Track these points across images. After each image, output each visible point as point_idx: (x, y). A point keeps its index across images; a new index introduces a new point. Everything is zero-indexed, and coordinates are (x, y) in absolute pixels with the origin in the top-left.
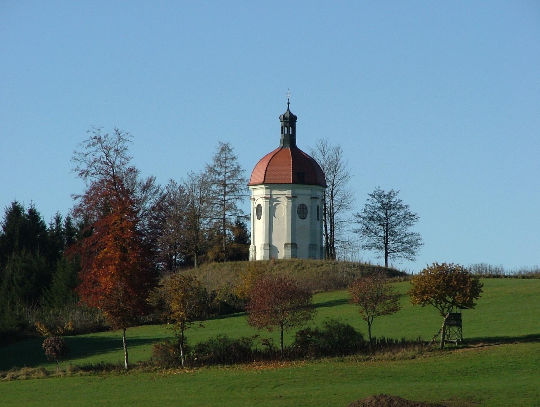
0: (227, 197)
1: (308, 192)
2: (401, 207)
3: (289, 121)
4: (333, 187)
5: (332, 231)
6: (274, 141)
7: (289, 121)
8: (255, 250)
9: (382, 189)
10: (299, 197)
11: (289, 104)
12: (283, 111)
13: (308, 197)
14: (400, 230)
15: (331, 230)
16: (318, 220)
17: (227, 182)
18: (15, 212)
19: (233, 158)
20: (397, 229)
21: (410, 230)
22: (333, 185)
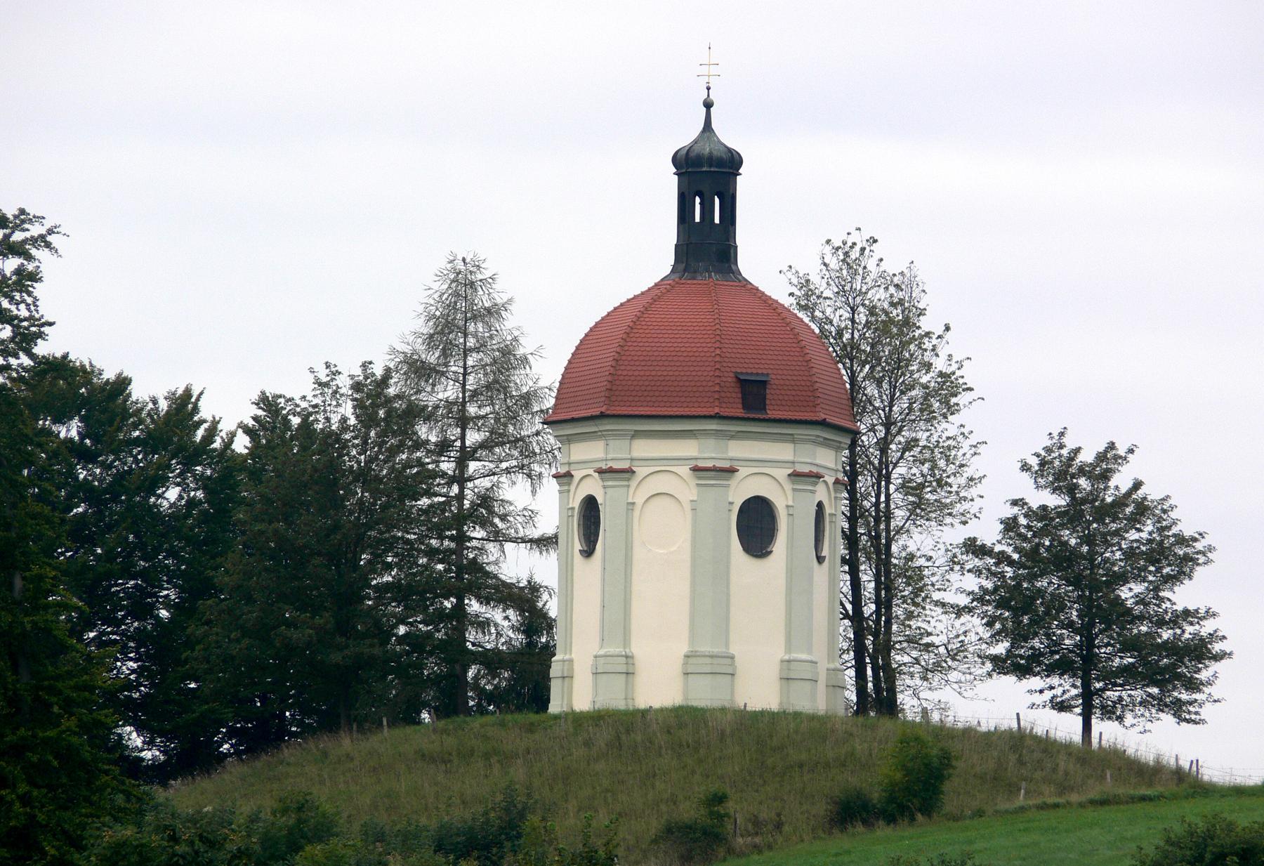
0: (473, 466)
1: (782, 451)
2: (1143, 509)
3: (707, 177)
4: (888, 432)
5: (884, 605)
6: (640, 248)
7: (707, 177)
8: (568, 677)
9: (1070, 443)
10: (743, 471)
11: (708, 105)
12: (686, 135)
13: (782, 473)
14: (1141, 601)
15: (878, 602)
16: (820, 559)
17: (472, 410)
18: (676, 160)
19: (155, 402)
20: (1129, 593)
21: (1182, 596)
22: (888, 424)
